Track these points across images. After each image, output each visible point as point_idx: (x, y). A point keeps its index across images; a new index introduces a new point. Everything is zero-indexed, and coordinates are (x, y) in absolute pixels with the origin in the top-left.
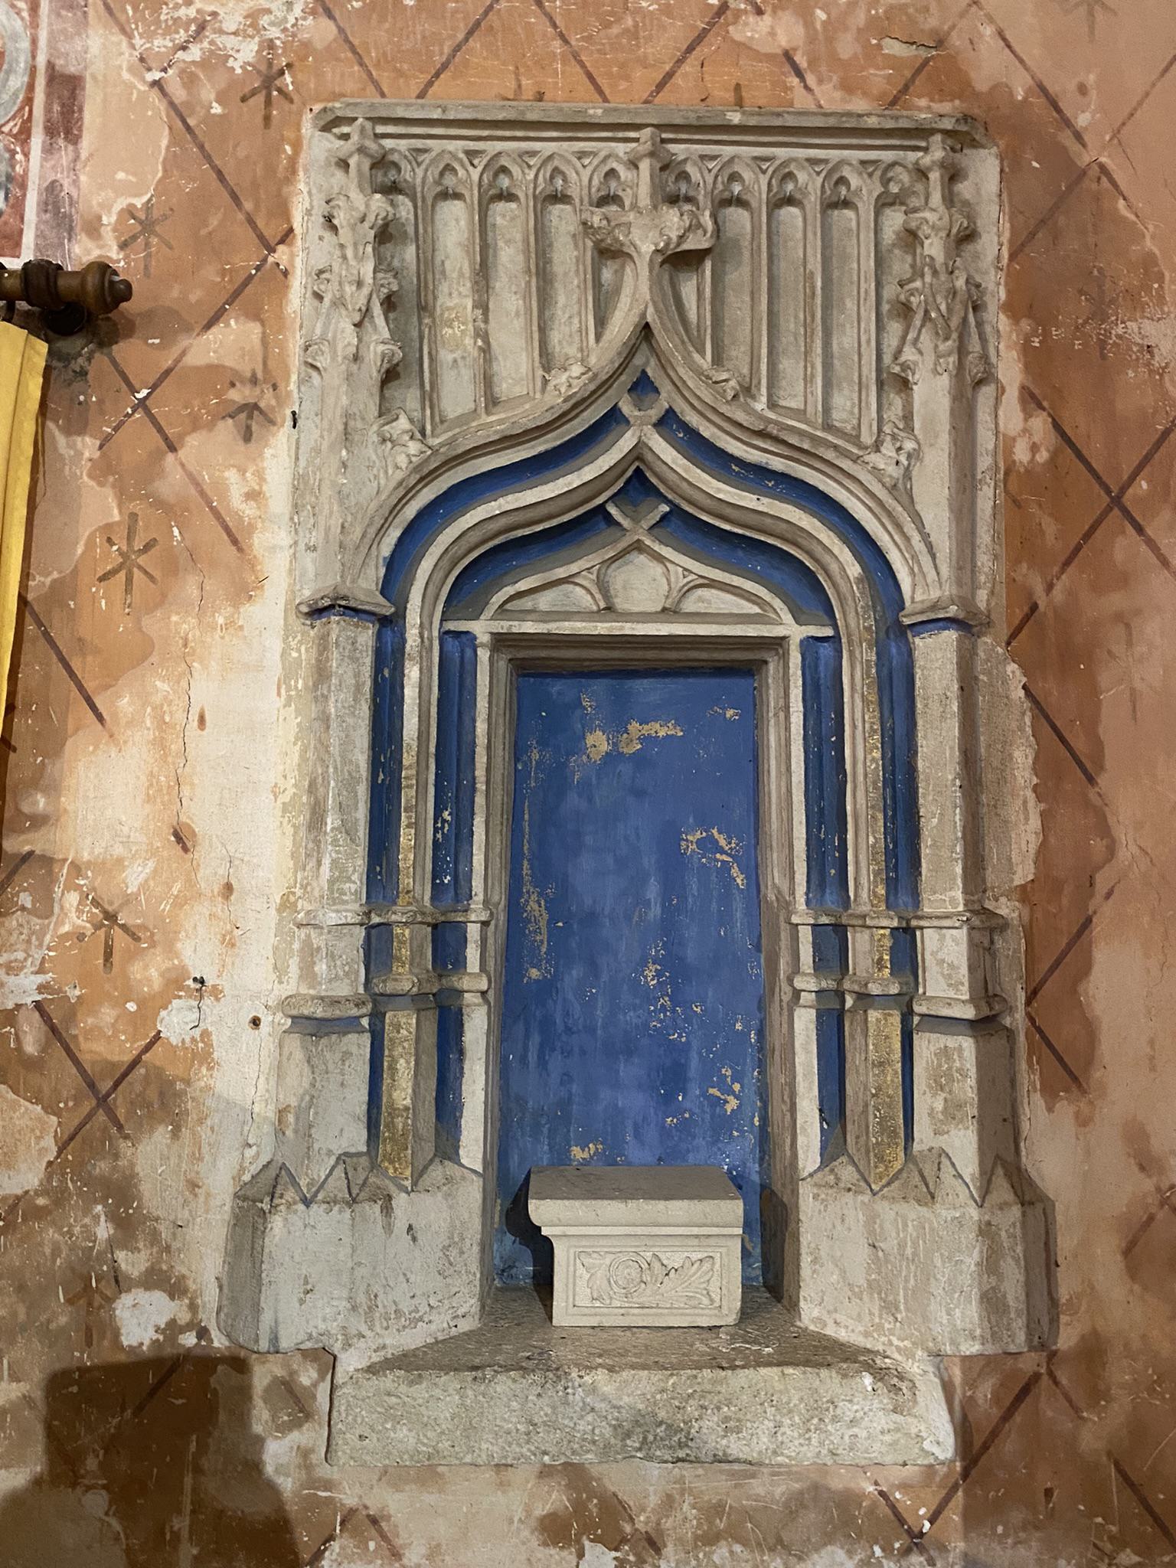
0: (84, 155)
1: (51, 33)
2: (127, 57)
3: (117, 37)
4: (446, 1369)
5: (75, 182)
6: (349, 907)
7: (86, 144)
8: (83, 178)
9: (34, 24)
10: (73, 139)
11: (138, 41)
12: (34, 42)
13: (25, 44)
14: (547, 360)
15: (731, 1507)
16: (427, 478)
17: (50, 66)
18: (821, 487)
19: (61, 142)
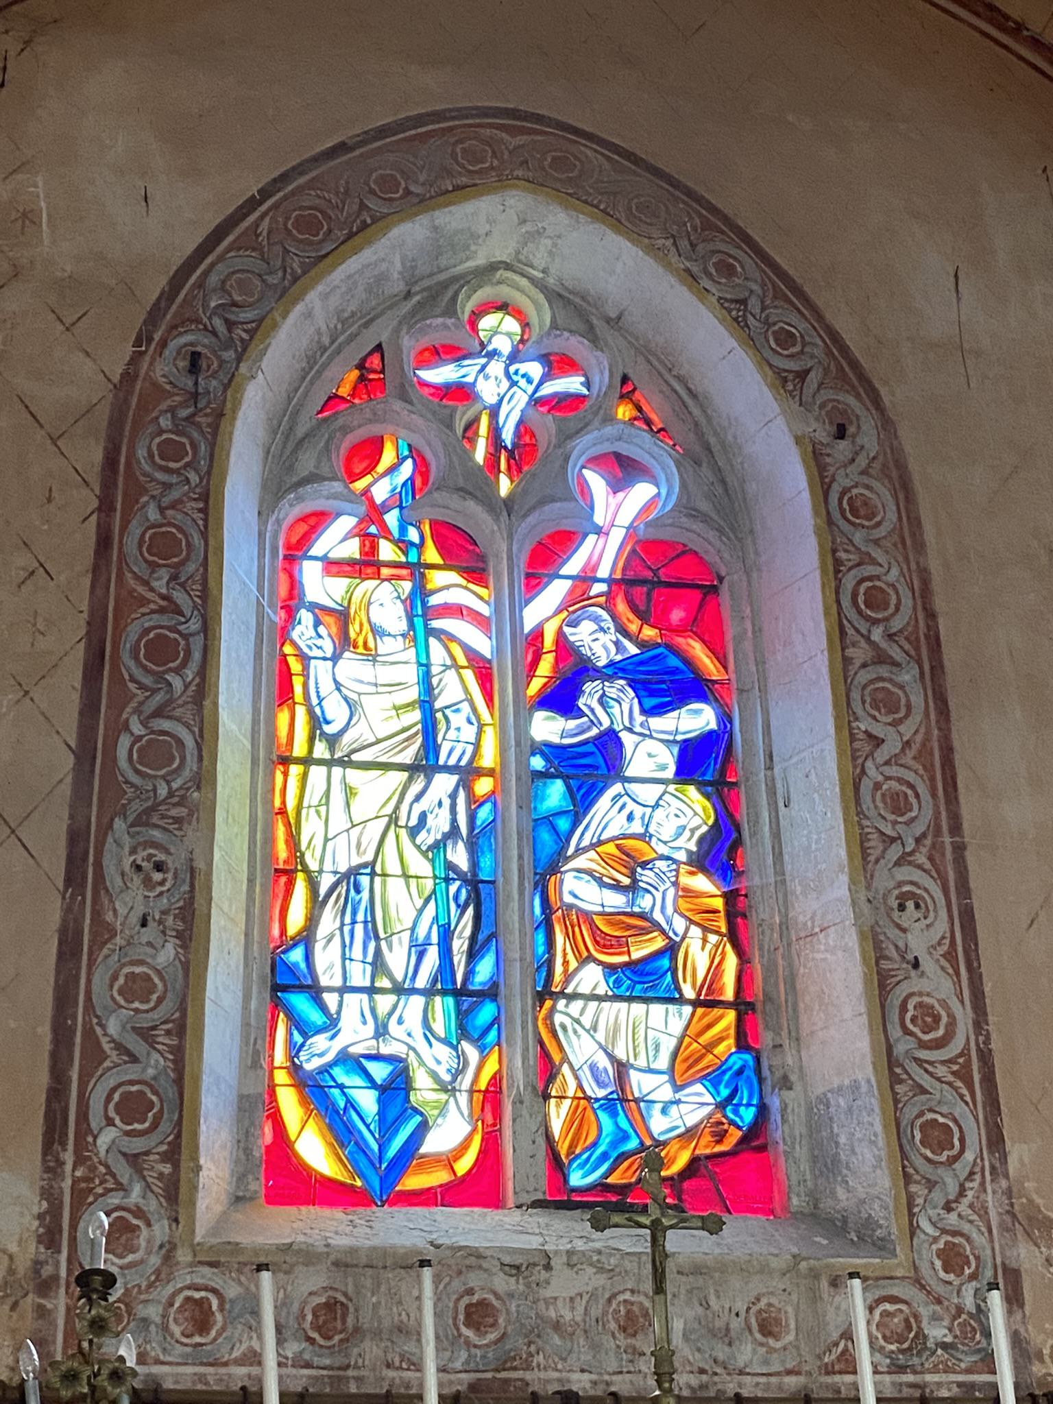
0: (1027, 1313)
1: (1001, 1245)
2: (1040, 1261)
3: (1033, 1248)
4: (1043, 44)
5: (1027, 1330)
6: (408, 981)
7: (1027, 1308)
8: (1030, 1328)
9: (992, 1241)
10: (1021, 1305)
11: (1043, 1249)
12: (993, 1249)
13: (989, 1252)
14: (487, 602)
15: (461, 393)
16: (275, 432)
17: (1003, 1264)
18: (357, 441)
19: (1015, 1308)
